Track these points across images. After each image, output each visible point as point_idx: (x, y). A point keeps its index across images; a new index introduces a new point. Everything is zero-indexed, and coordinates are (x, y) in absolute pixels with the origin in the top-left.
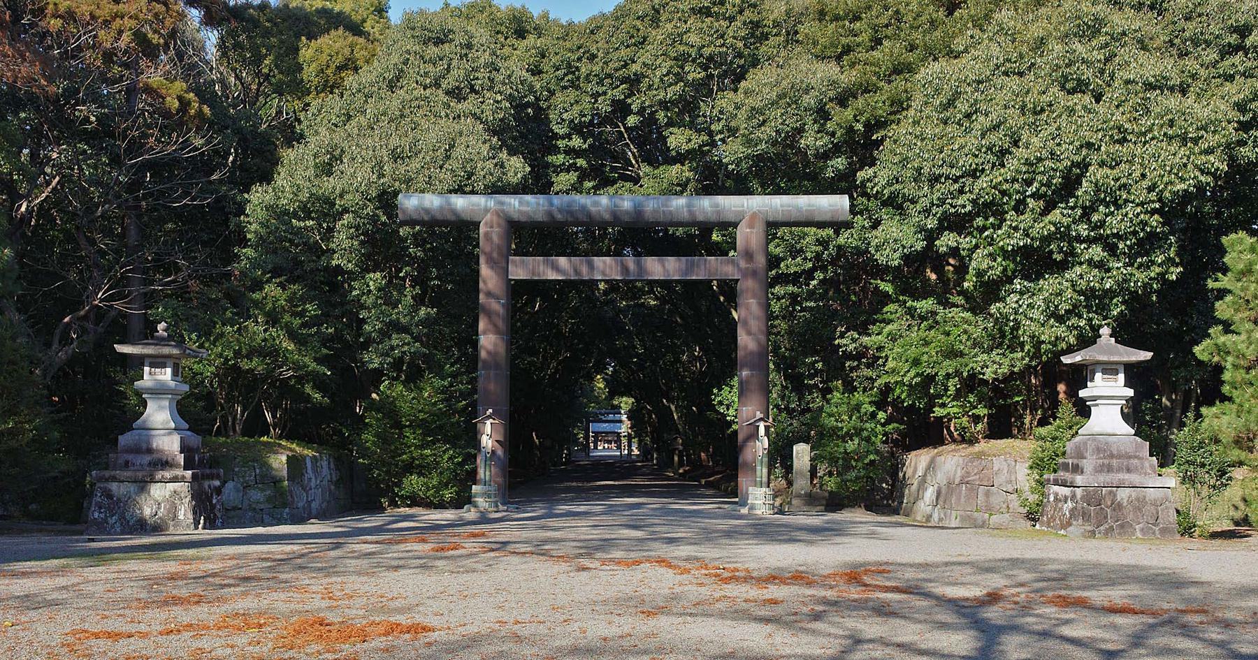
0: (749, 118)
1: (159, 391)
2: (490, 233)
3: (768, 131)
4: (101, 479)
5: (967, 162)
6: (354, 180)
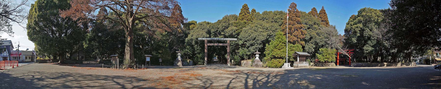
2: (206, 41)
6: (194, 37)
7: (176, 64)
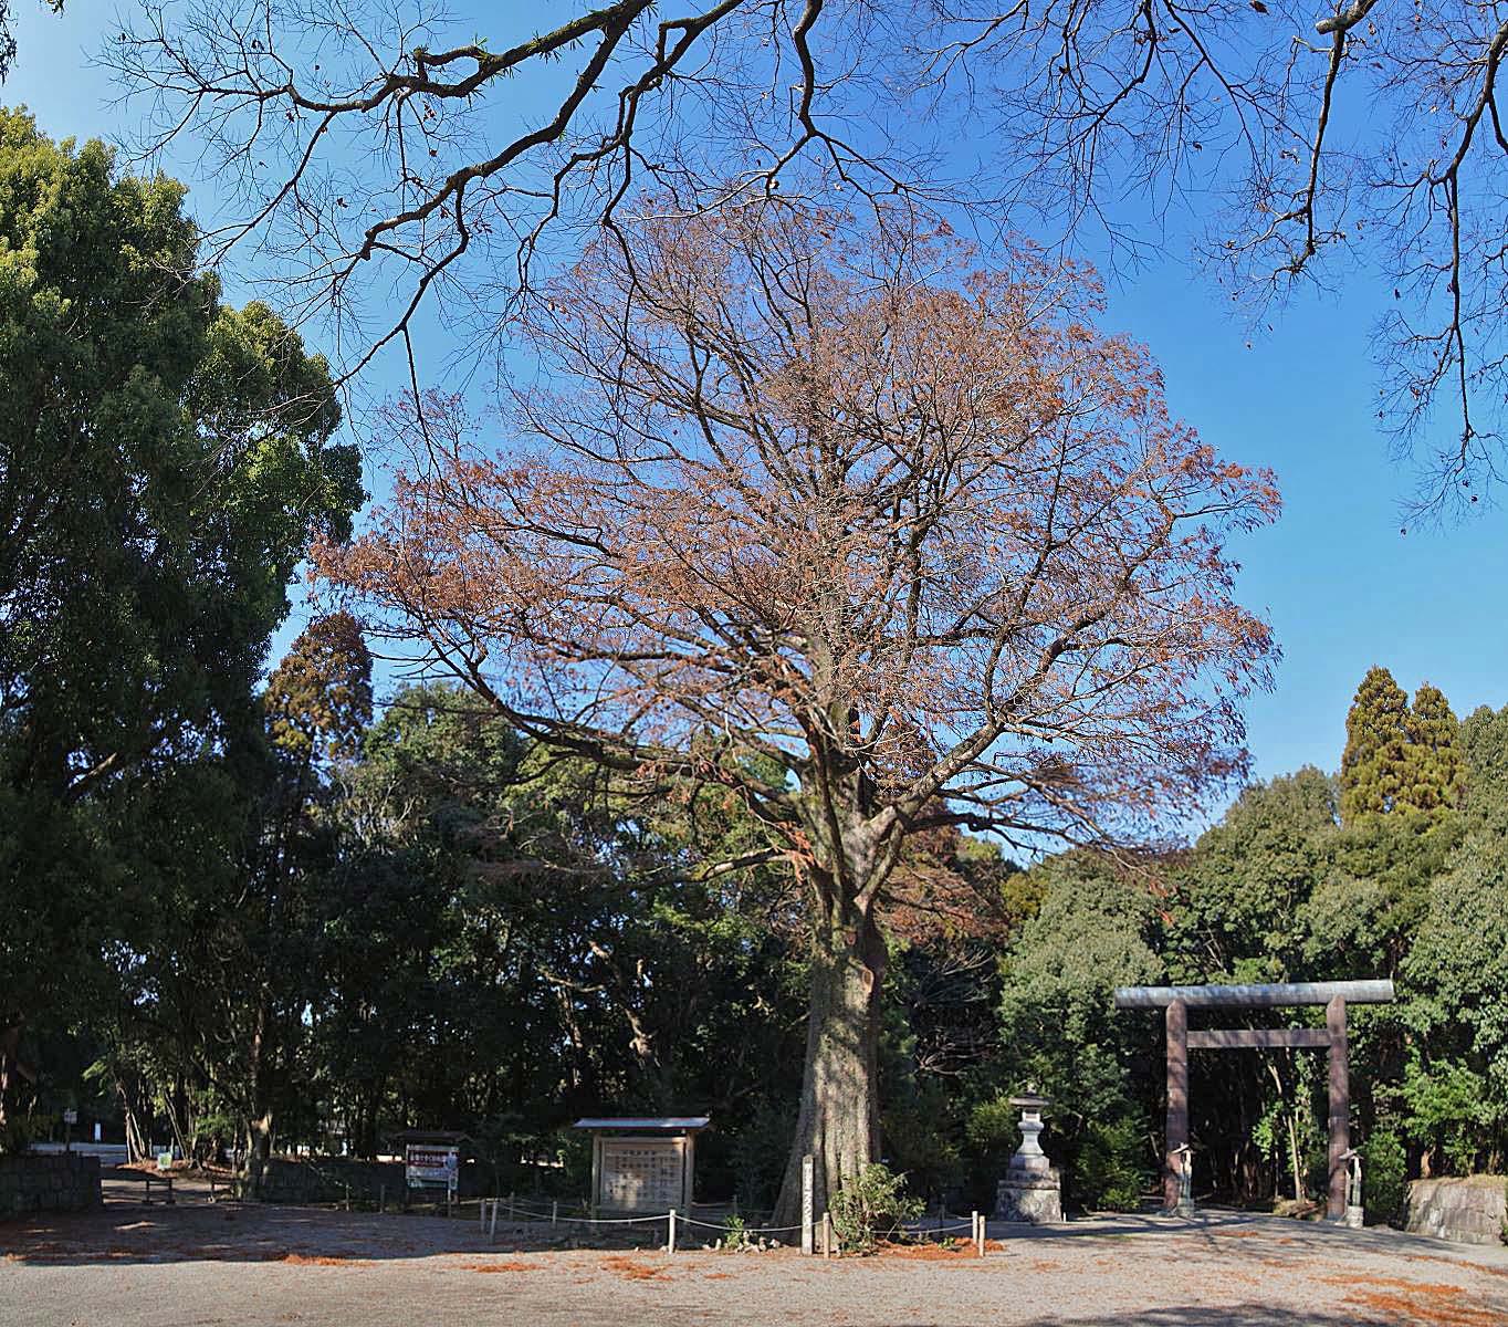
0: (1325, 924)
1: (1031, 1129)
2: (1174, 1015)
3: (1337, 933)
4: (1004, 1186)
5: (1477, 955)
6: (1078, 979)
7: (1012, 1203)
